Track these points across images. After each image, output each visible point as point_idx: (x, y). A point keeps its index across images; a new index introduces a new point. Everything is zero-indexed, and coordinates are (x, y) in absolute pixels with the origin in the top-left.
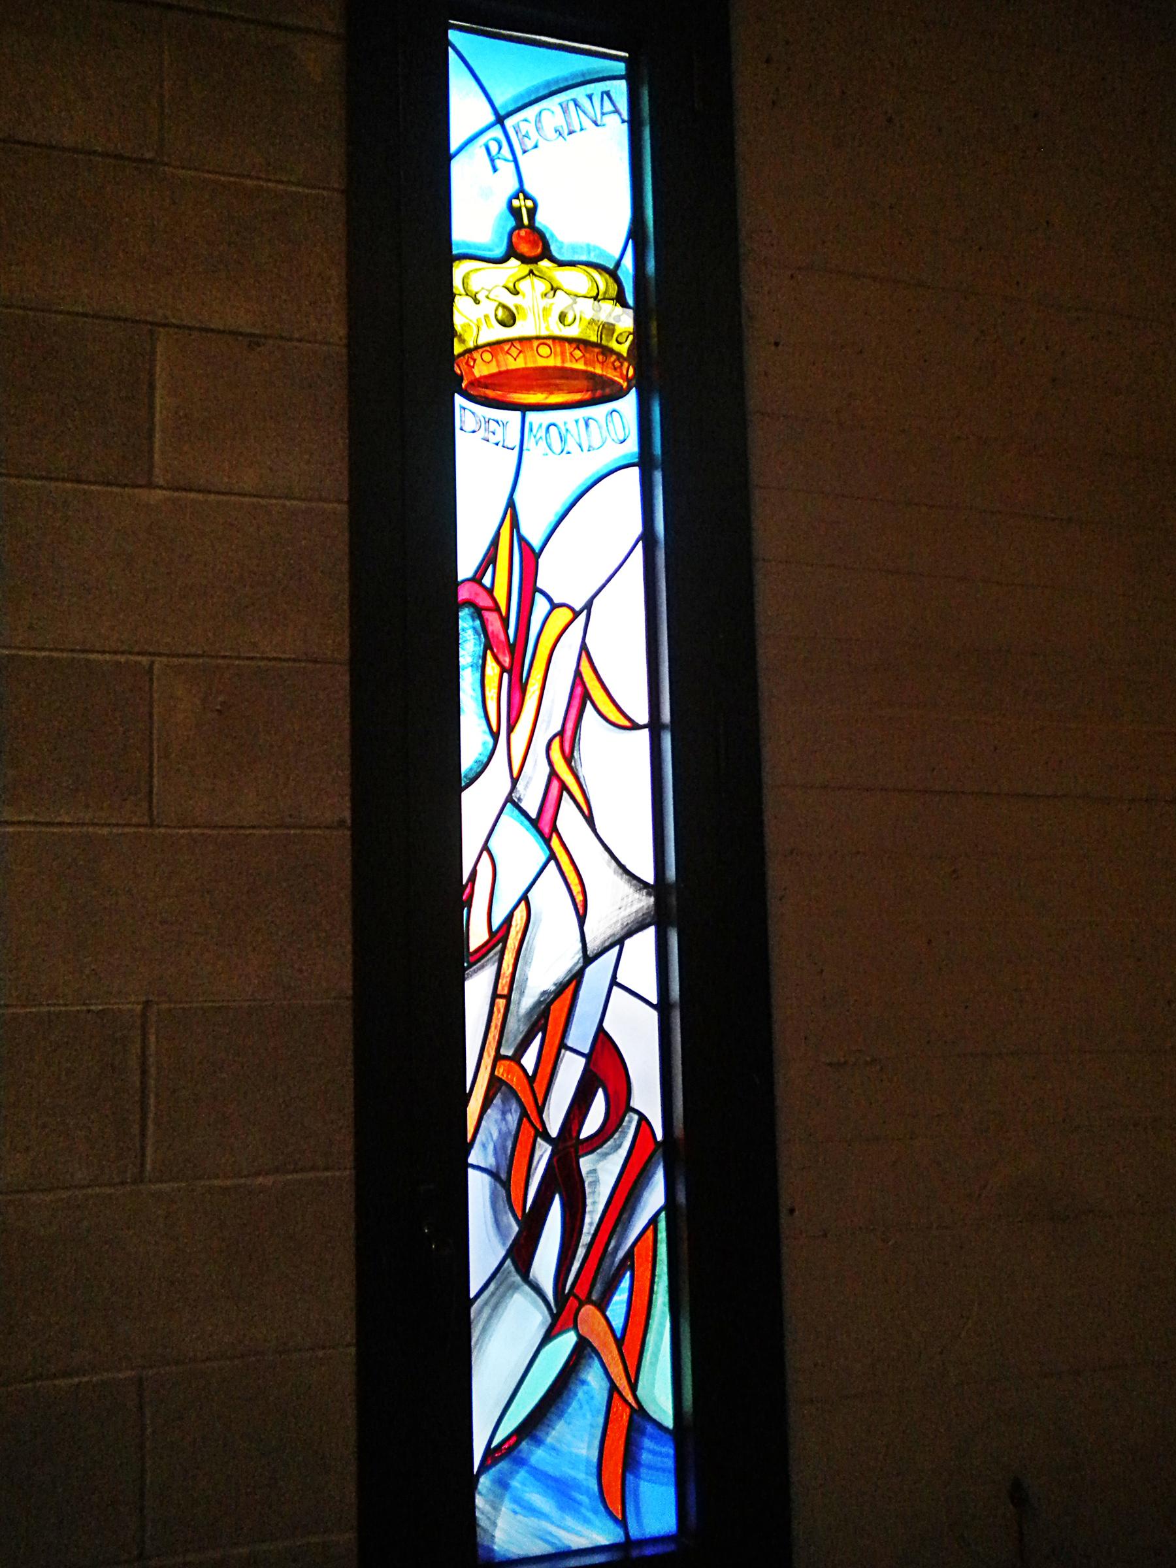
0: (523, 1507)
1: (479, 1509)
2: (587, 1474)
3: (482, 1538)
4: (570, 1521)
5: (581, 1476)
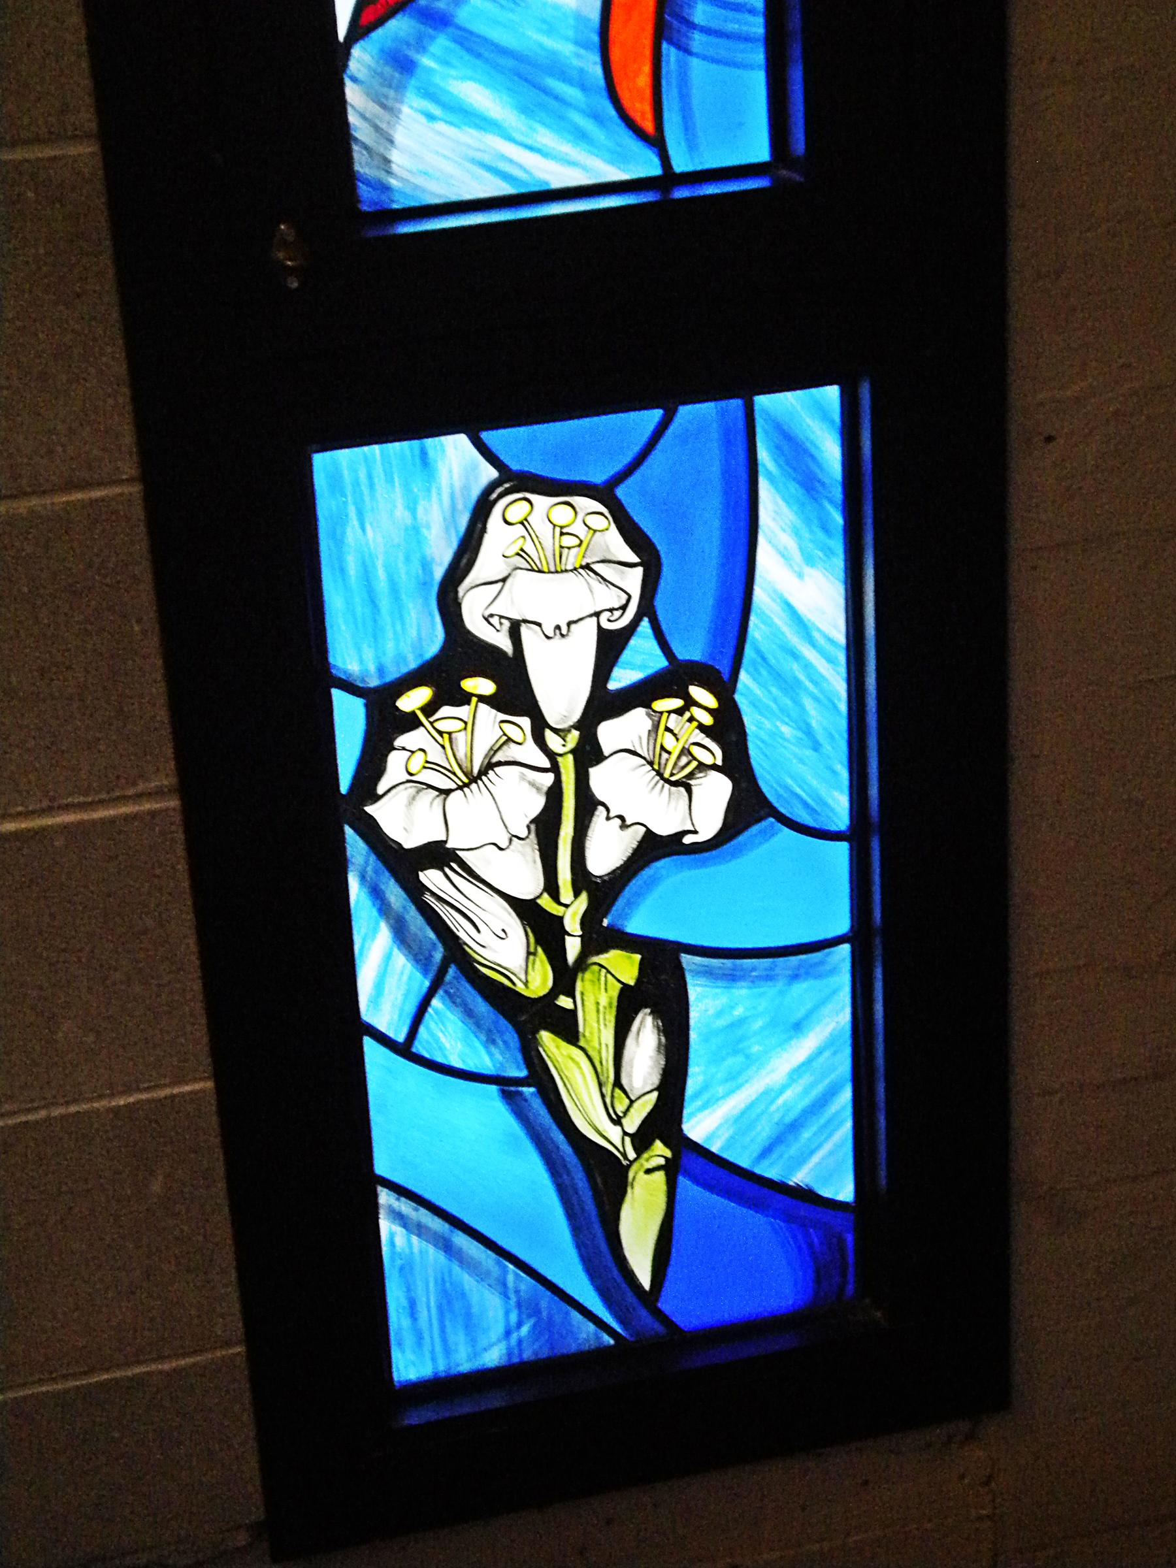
0: (444, 106)
1: (352, 106)
2: (577, 43)
3: (362, 164)
4: (545, 137)
5: (565, 49)
